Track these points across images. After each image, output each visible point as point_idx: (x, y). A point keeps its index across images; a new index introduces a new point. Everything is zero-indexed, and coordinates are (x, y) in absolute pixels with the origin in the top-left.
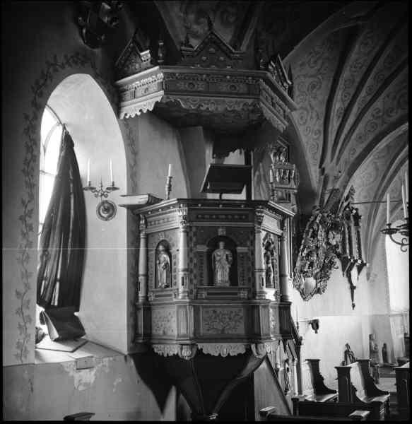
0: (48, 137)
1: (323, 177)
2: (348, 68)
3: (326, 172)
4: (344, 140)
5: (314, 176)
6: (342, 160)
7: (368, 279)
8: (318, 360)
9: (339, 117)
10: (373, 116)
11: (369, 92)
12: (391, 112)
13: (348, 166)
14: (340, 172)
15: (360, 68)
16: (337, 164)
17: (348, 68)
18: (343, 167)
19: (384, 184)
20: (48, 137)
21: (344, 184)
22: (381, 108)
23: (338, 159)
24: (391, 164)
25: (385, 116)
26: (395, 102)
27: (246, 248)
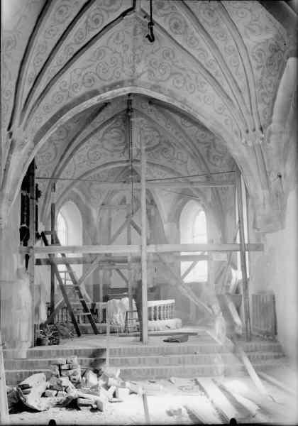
0: (90, 346)
1: (10, 140)
2: (43, 33)
3: (13, 136)
4: (33, 108)
5: (158, 32)
6: (29, 126)
7: (167, 326)
8: (10, 412)
9: (30, 82)
10: (60, 88)
11: (59, 63)
12: (76, 87)
13: (34, 134)
14: (26, 138)
15: (54, 35)
16: (24, 129)
17: (43, 33)
18: (31, 137)
19: (61, 165)
20: (90, 346)
21: (30, 151)
22: (68, 82)
23: (26, 125)
24: (68, 147)
25: (71, 91)
26: (80, 79)
27: (25, 357)
